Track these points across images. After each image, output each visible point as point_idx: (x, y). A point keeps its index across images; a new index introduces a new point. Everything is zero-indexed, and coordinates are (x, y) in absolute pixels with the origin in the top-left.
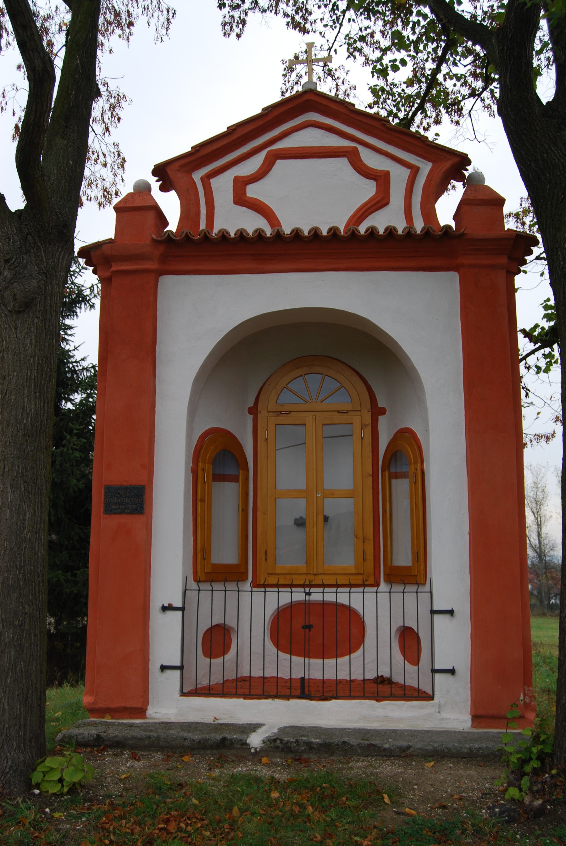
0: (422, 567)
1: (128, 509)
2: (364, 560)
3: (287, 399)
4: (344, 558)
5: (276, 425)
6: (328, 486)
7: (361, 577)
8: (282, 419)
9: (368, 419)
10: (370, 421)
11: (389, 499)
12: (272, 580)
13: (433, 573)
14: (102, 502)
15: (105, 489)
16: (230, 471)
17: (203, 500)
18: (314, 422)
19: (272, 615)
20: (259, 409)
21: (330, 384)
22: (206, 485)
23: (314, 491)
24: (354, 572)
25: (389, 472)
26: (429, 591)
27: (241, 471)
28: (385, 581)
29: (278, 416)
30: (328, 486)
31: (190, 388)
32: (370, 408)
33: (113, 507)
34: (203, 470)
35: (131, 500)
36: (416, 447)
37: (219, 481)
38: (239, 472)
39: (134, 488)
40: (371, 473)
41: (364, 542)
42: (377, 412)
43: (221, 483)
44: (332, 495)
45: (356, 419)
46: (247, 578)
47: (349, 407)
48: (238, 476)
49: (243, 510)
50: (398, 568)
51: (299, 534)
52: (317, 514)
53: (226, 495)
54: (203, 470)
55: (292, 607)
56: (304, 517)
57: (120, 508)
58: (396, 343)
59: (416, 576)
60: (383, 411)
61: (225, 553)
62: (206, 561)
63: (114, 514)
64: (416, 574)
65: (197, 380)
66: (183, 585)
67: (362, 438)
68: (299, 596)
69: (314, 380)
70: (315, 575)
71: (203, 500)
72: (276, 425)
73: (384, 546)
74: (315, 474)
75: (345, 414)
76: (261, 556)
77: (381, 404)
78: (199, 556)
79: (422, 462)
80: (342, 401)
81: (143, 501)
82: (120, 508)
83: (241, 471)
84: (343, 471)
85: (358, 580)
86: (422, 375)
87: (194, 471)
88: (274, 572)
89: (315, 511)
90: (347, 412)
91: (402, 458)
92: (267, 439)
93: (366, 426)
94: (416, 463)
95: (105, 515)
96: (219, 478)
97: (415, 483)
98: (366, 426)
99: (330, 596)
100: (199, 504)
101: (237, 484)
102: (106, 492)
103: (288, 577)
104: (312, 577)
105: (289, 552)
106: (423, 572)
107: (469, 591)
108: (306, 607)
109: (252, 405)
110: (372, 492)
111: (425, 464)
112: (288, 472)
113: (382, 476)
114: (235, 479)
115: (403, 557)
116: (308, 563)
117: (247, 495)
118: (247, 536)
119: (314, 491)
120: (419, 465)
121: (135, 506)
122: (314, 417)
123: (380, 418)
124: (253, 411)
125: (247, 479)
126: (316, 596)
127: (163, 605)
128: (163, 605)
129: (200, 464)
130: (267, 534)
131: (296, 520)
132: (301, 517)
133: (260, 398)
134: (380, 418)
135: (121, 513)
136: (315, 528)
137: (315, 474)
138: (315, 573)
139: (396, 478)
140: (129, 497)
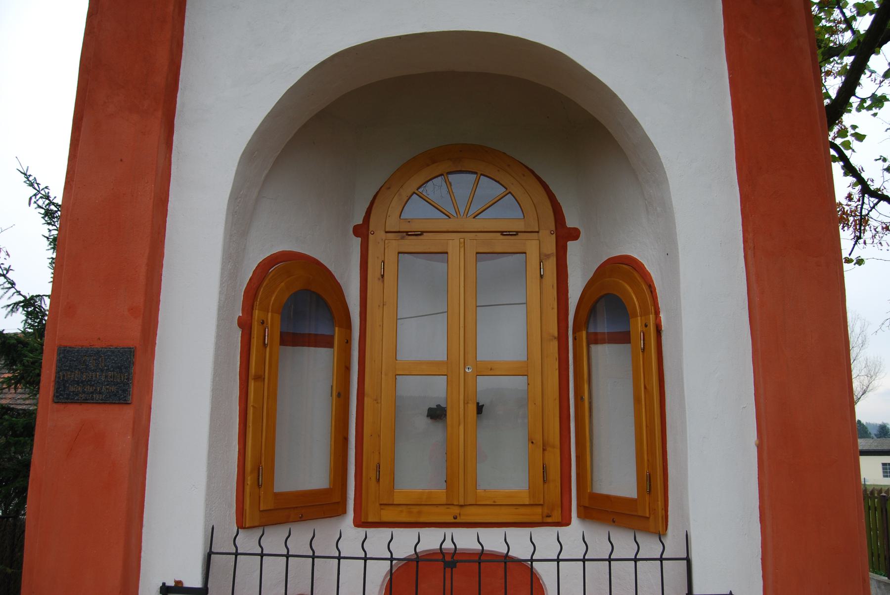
0: (660, 503)
1: (100, 393)
2: (544, 482)
3: (417, 212)
4: (506, 471)
5: (399, 253)
6: (484, 355)
7: (539, 510)
8: (411, 244)
9: (550, 246)
10: (555, 251)
11: (585, 379)
12: (388, 515)
13: (692, 522)
14: (53, 378)
15: (59, 354)
16: (323, 330)
17: (259, 378)
18: (462, 250)
19: (382, 585)
20: (371, 229)
21: (489, 189)
22: (268, 349)
23: (462, 361)
24: (527, 503)
25: (587, 333)
26: (685, 556)
27: (337, 329)
28: (579, 516)
29: (403, 238)
30: (484, 355)
31: (235, 169)
32: (553, 228)
33: (72, 389)
34: (263, 323)
35: (106, 377)
36: (644, 287)
37: (309, 346)
38: (334, 331)
39: (113, 352)
40: (556, 334)
41: (544, 450)
42: (565, 235)
43: (312, 349)
44: (490, 370)
45: (532, 247)
46: (344, 512)
47: (520, 226)
48: (332, 337)
49: (339, 395)
50: (608, 498)
51: (435, 433)
52: (466, 403)
53: (309, 375)
54: (263, 323)
55: (418, 562)
56: (443, 405)
57: (84, 392)
58: (614, 96)
59: (648, 518)
60: (574, 234)
61: (305, 466)
62: (262, 489)
63: (74, 402)
64: (647, 515)
65: (251, 155)
66: (205, 543)
67: (541, 276)
68: (431, 540)
69: (462, 183)
70: (461, 506)
71: (259, 378)
72: (399, 253)
73: (577, 457)
74: (463, 338)
75: (513, 237)
76: (369, 473)
77: (570, 223)
78: (249, 480)
79: (657, 313)
80: (508, 214)
81: (128, 379)
82: (84, 392)
83: (337, 329)
84: (510, 333)
85: (536, 514)
86: (661, 153)
87: (245, 325)
88: (391, 502)
89: (462, 397)
90: (517, 233)
91: (618, 307)
92: (383, 276)
93: (548, 256)
94: (645, 313)
95: (55, 405)
96: (291, 339)
97: (643, 350)
98: (548, 256)
99: (493, 541)
100: (252, 384)
101: (629, 345)
102: (59, 361)
103: (415, 509)
104: (456, 510)
105: (417, 471)
106: (661, 512)
107: (760, 556)
108: (449, 561)
109: (361, 222)
110: (557, 367)
111: (661, 315)
112: (415, 333)
113: (575, 339)
114: (326, 342)
115: (617, 477)
116: (450, 482)
117: (348, 369)
118: (346, 439)
119: (462, 361)
120: (652, 317)
121: (114, 389)
122: (462, 240)
123: (571, 245)
124: (362, 231)
125: (348, 342)
126: (466, 540)
127: (164, 584)
128: (164, 584)
129: (256, 313)
130: (379, 436)
131: (430, 410)
132: (438, 406)
133: (373, 212)
134: (571, 245)
135: (85, 401)
136: (462, 427)
137: (463, 338)
138: (462, 503)
139: (596, 342)
140: (102, 371)
